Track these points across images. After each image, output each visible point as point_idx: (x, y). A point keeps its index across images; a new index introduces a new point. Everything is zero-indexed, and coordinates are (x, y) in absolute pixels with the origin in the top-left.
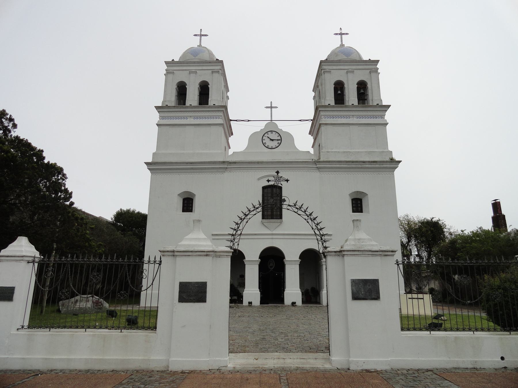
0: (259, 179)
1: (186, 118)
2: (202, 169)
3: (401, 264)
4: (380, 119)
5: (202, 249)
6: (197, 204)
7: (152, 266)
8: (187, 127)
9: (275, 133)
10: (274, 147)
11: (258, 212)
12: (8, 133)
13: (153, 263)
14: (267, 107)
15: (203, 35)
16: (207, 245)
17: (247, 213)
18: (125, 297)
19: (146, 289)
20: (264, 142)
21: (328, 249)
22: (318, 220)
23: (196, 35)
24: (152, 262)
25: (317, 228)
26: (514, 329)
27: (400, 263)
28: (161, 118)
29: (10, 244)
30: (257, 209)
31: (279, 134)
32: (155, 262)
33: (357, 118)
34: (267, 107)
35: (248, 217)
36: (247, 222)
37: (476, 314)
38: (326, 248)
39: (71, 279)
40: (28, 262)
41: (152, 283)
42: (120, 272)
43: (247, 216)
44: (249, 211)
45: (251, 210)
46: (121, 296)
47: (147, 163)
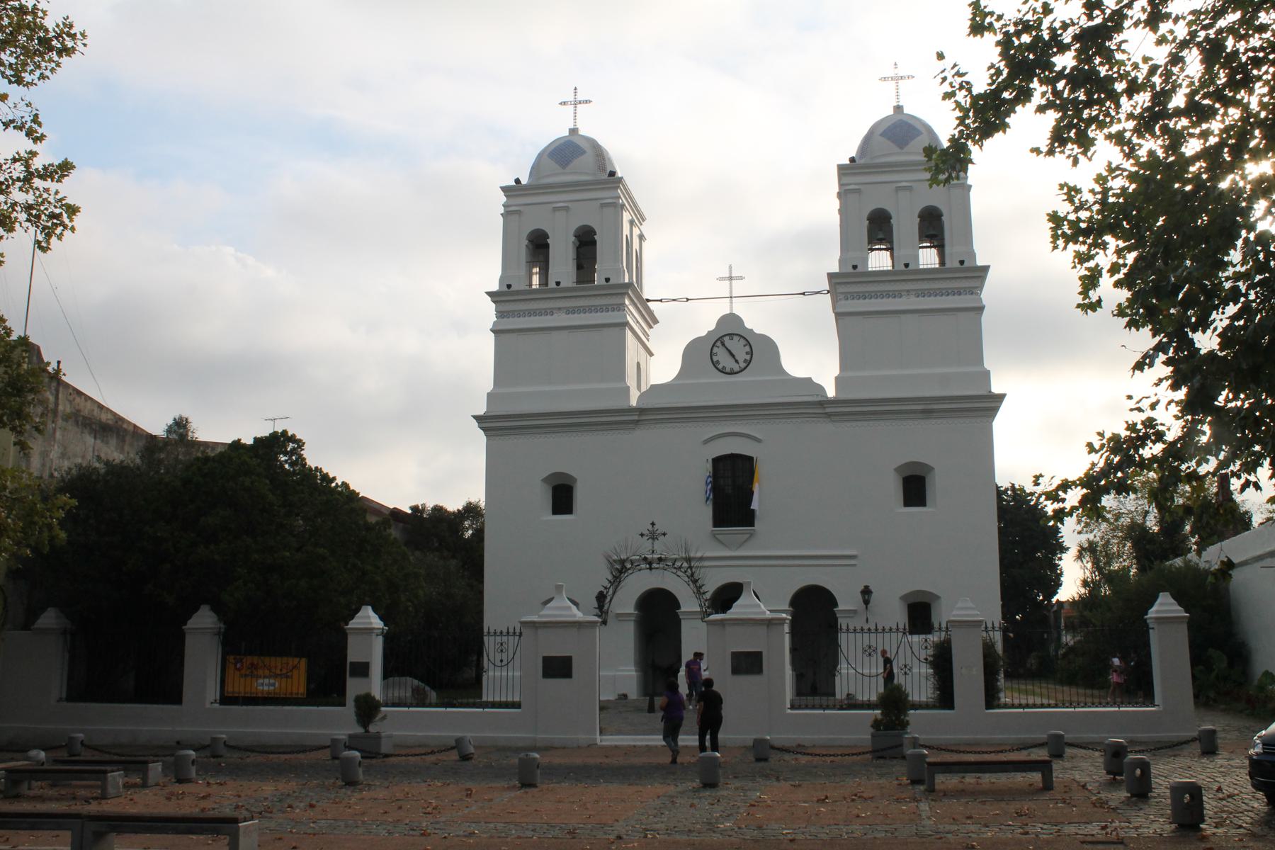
0: (706, 442)
1: (550, 312)
2: (555, 427)
4: (969, 297)
6: (581, 497)
7: (511, 638)
8: (554, 334)
9: (738, 338)
10: (743, 342)
12: (962, 156)
14: (721, 279)
15: (580, 102)
20: (715, 358)
23: (564, 103)
24: (852, 631)
28: (501, 314)
29: (735, 602)
31: (747, 340)
32: (898, 630)
33: (918, 296)
34: (721, 279)
37: (1014, 686)
40: (377, 635)
47: (476, 418)
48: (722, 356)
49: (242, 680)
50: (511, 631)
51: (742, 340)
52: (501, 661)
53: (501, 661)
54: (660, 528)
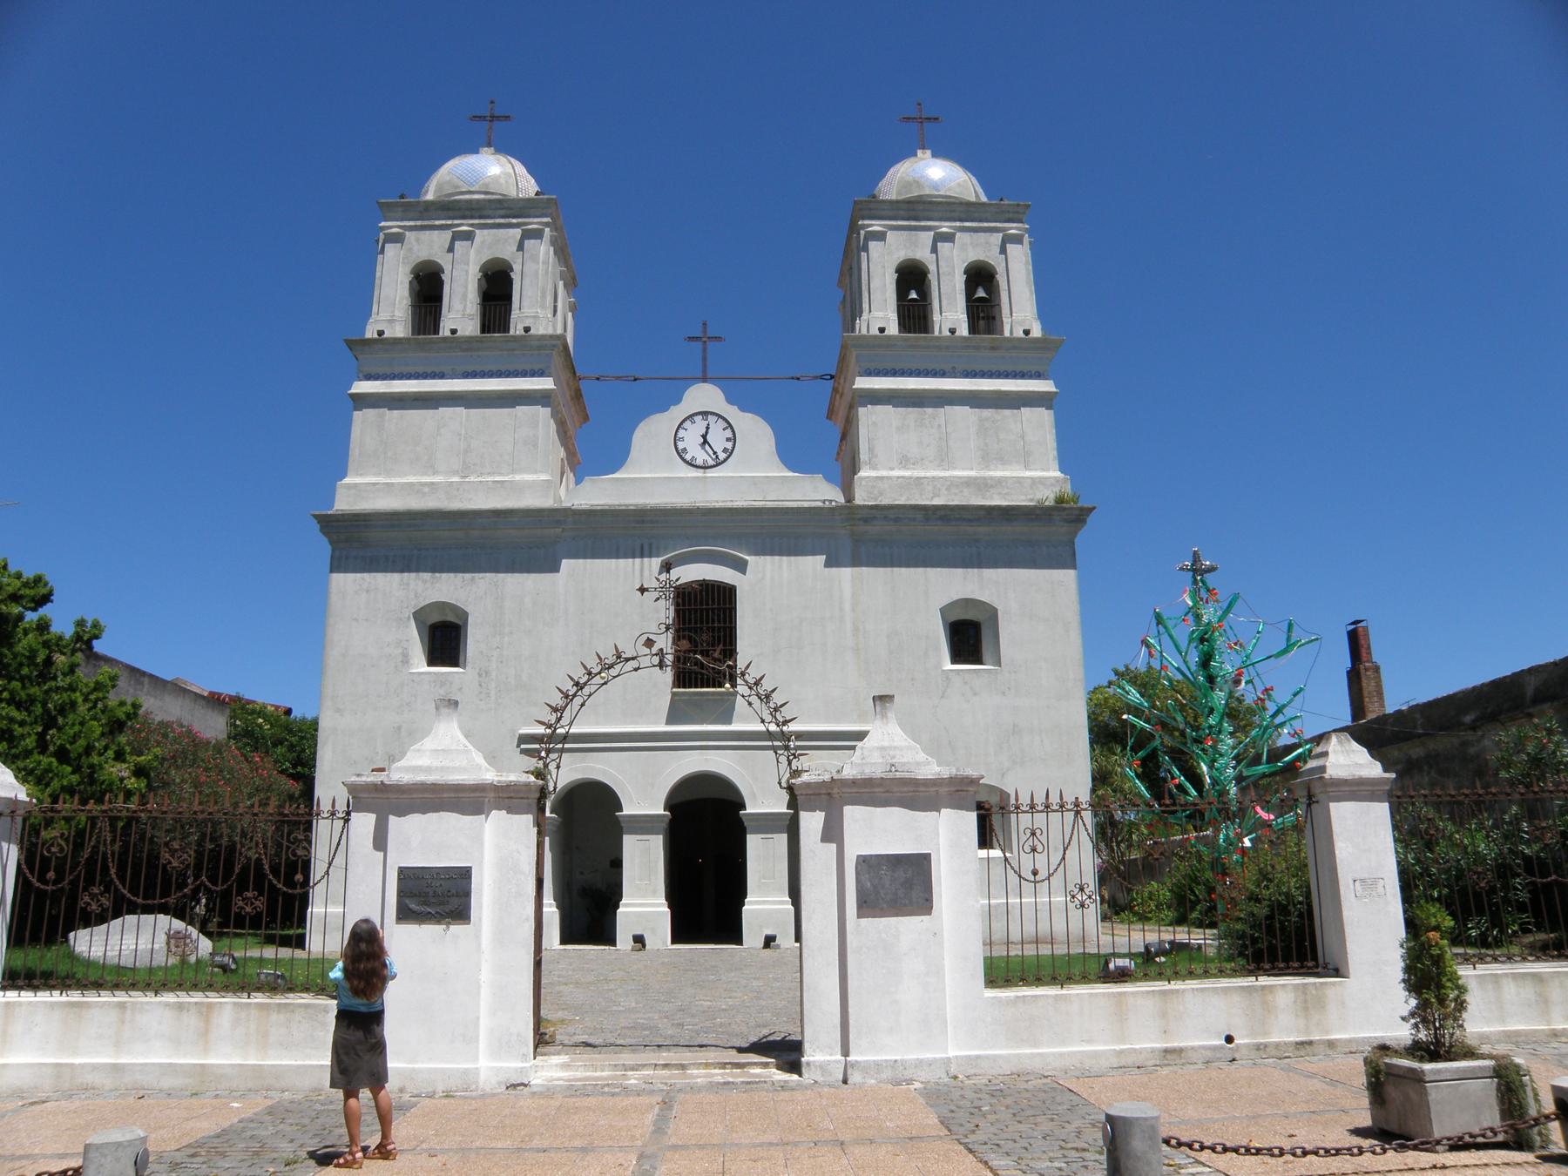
3: (1086, 810)
5: (458, 777)
7: (1055, 817)
11: (614, 677)
13: (327, 818)
16: (477, 769)
17: (582, 681)
18: (255, 908)
19: (1020, 876)
21: (805, 778)
22: (777, 699)
24: (326, 815)
25: (776, 719)
26: (1267, 966)
27: (1084, 806)
30: (609, 668)
35: (586, 690)
36: (582, 705)
38: (796, 773)
39: (113, 861)
41: (328, 871)
42: (89, 844)
43: (582, 688)
44: (590, 673)
45: (594, 671)
46: (246, 904)
48: (718, 439)
49: (1044, 927)
50: (1054, 800)
51: (685, 425)
52: (1035, 873)
53: (1035, 873)
54: (639, 593)
